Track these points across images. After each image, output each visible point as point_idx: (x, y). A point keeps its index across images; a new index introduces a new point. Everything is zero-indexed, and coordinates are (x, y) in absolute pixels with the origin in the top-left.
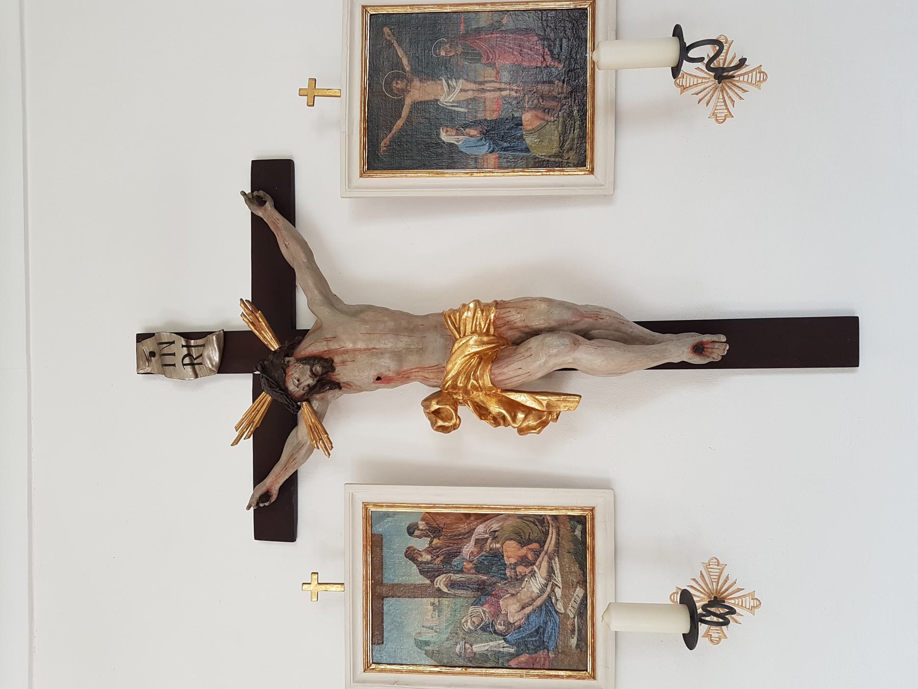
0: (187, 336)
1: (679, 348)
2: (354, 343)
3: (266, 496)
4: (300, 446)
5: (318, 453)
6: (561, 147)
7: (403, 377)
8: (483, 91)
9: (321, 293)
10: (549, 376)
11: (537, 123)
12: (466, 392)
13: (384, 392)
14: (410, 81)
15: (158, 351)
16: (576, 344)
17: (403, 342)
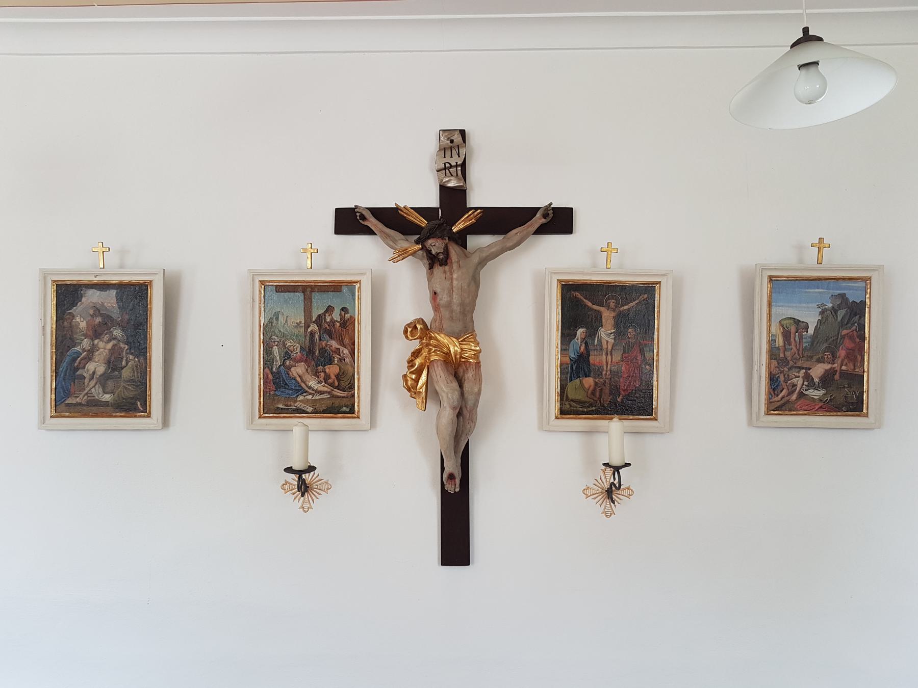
0: (463, 165)
1: (452, 466)
2: (457, 279)
3: (363, 217)
4: (395, 241)
5: (390, 253)
6: (572, 400)
7: (436, 308)
8: (607, 354)
9: (487, 257)
10: (437, 393)
11: (587, 386)
12: (428, 345)
13: (427, 295)
14: (614, 311)
15: (455, 143)
16: (454, 408)
17: (456, 308)
